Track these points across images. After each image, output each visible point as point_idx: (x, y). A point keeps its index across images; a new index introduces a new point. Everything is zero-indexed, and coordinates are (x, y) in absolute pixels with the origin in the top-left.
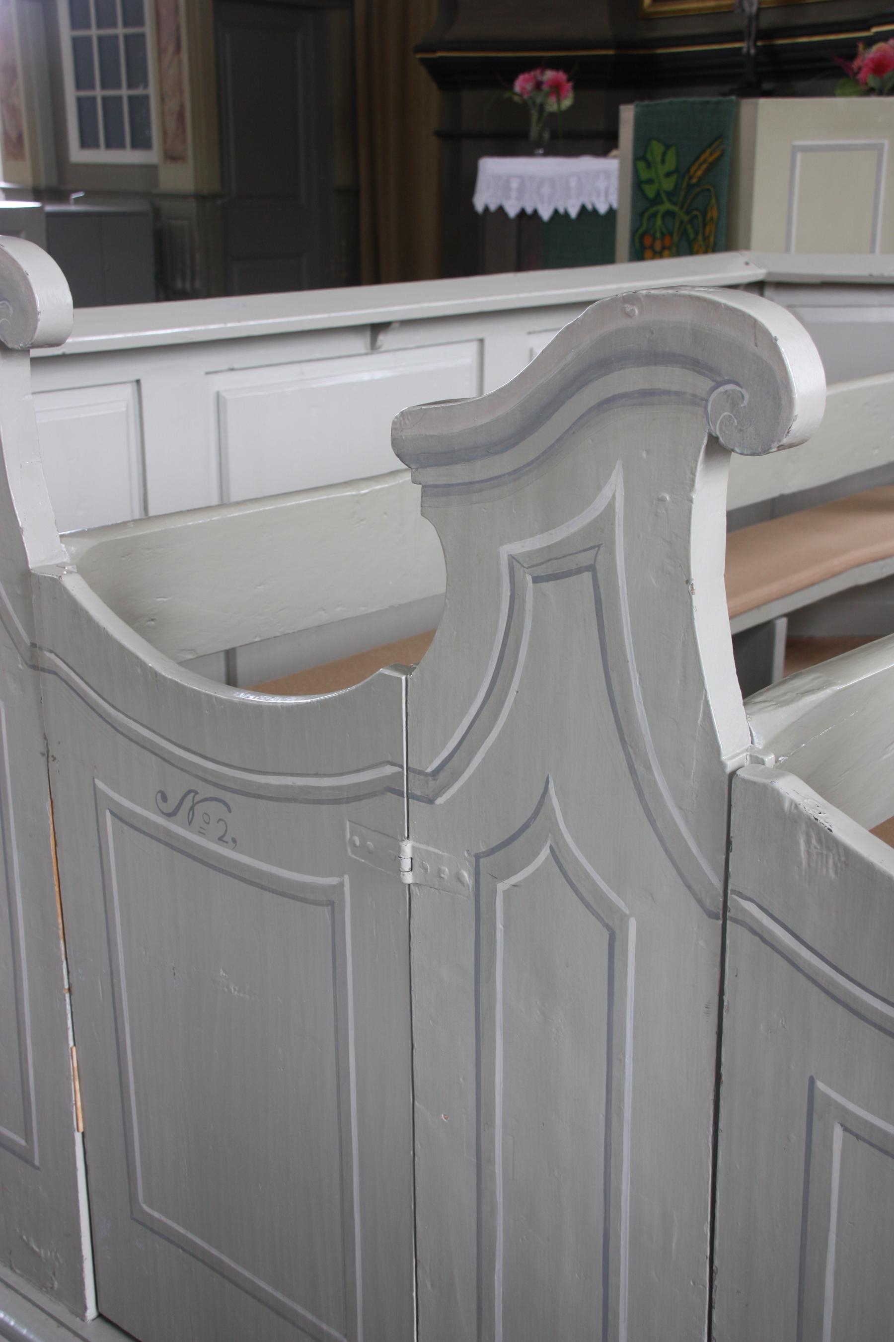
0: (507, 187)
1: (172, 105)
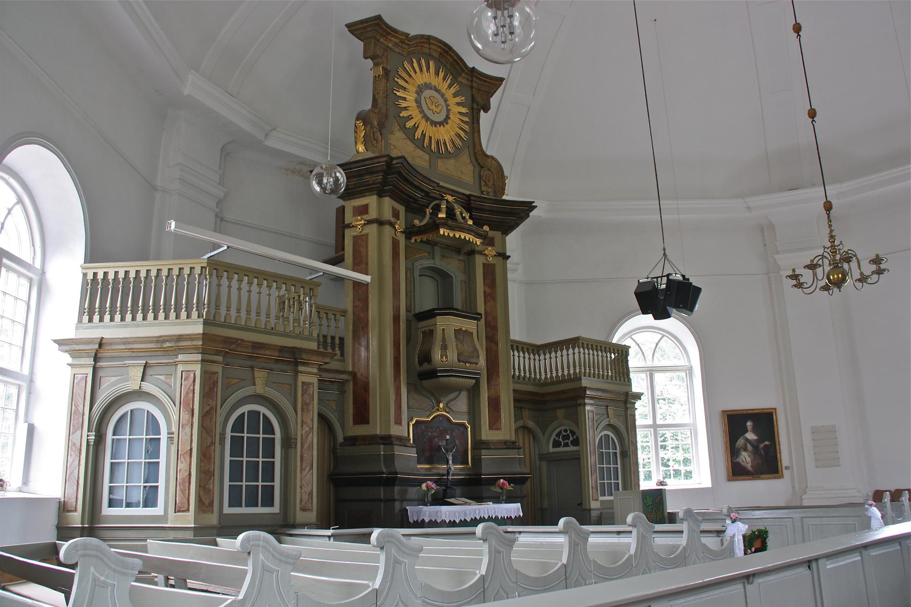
0: (465, 514)
1: (308, 489)
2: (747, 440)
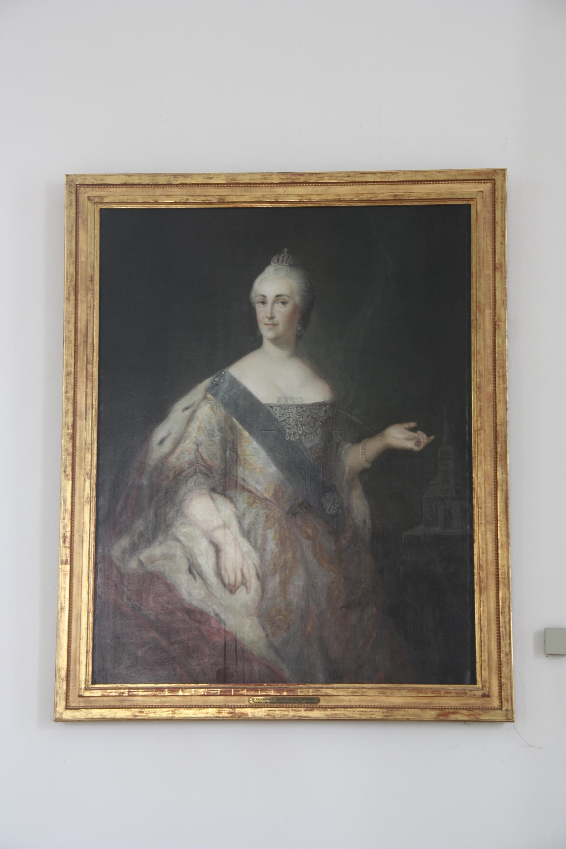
2: (246, 410)
